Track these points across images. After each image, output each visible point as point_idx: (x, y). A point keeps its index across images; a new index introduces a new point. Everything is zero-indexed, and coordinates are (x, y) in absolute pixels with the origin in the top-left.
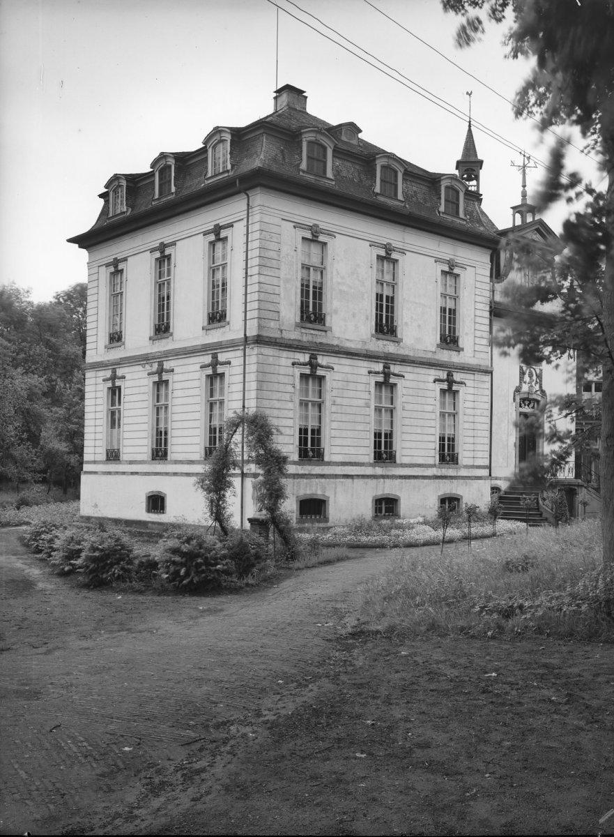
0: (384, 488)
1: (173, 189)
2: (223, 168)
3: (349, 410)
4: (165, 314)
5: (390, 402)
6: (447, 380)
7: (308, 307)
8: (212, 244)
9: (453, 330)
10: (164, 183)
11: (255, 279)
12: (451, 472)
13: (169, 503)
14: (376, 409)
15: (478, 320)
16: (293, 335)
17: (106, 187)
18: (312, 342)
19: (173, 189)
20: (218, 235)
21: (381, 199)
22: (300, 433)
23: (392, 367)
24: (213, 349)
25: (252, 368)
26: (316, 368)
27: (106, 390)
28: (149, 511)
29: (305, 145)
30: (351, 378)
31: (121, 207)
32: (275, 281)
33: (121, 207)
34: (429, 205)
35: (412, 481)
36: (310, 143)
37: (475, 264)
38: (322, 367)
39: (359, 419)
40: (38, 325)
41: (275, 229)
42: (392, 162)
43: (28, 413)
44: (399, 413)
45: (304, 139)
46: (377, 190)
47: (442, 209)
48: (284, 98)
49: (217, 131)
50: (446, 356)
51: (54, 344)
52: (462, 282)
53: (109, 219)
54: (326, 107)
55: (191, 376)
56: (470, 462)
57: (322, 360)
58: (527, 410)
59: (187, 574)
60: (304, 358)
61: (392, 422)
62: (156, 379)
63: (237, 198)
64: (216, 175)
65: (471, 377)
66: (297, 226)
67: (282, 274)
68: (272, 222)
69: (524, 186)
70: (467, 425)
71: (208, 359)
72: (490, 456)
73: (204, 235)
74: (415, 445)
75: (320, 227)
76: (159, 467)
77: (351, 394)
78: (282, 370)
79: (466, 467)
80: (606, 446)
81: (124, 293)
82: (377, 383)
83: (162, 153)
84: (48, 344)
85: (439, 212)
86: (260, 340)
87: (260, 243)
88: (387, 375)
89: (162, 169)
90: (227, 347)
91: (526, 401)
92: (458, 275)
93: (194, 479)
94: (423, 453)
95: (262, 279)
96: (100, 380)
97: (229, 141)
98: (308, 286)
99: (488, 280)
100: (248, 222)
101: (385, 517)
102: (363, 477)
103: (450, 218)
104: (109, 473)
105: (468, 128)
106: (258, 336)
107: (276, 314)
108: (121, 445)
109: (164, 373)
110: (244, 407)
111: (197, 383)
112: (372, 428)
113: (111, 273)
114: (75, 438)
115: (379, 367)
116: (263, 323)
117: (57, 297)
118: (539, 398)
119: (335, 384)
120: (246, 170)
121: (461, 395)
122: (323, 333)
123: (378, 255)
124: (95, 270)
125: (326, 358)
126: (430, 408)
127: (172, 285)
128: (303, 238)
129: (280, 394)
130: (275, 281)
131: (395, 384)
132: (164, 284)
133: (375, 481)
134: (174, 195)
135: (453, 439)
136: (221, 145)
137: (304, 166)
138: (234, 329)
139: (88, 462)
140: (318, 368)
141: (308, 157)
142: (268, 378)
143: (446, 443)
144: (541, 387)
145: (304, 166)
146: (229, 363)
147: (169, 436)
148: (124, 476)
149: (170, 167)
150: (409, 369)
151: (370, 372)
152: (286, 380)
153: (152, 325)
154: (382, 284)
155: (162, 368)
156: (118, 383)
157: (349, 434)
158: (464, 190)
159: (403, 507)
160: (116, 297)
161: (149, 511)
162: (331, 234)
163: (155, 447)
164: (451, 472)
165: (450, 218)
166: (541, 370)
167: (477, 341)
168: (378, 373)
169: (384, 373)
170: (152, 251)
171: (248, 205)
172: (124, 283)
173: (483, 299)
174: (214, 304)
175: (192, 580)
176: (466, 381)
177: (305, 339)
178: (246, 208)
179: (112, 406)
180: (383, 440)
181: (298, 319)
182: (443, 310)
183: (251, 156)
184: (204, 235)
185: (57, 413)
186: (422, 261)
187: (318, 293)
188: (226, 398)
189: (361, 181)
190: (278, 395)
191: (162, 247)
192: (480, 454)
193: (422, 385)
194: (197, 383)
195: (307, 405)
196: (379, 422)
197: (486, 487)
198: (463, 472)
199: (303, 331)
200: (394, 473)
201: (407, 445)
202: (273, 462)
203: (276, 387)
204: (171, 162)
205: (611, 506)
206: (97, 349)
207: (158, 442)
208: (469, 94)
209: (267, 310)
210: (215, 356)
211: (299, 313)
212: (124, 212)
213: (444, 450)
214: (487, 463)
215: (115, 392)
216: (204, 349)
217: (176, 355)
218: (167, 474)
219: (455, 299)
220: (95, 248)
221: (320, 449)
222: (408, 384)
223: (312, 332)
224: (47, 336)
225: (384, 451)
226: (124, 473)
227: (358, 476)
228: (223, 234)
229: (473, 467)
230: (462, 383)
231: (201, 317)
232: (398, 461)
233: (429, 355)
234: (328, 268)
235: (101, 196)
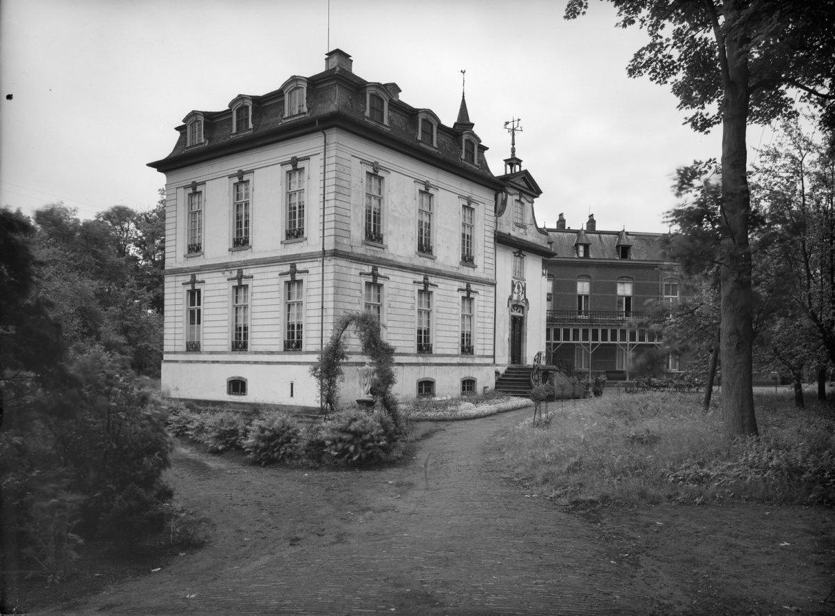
1: (251, 126)
3: (400, 312)
7: (370, 228)
10: (242, 121)
11: (332, 203)
13: (249, 387)
15: (487, 244)
16: (360, 250)
17: (184, 121)
18: (373, 257)
19: (251, 126)
20: (295, 167)
21: (422, 145)
24: (292, 260)
26: (377, 278)
27: (185, 292)
28: (229, 393)
29: (368, 96)
30: (401, 286)
32: (347, 206)
34: (453, 153)
35: (443, 367)
36: (372, 95)
37: (484, 200)
38: (381, 277)
39: (407, 318)
40: (85, 238)
43: (85, 311)
44: (434, 315)
46: (419, 138)
47: (463, 157)
49: (294, 79)
50: (466, 271)
51: (101, 254)
54: (366, 69)
55: (270, 282)
57: (381, 271)
58: (516, 313)
59: (356, 451)
60: (368, 269)
62: (236, 283)
63: (313, 136)
65: (482, 288)
66: (363, 162)
68: (344, 157)
70: (479, 325)
71: (287, 268)
72: (494, 347)
74: (445, 341)
77: (402, 299)
78: (353, 279)
80: (729, 341)
84: (94, 253)
85: (461, 159)
88: (426, 284)
89: (239, 108)
90: (306, 259)
92: (473, 209)
93: (308, 368)
94: (450, 346)
95: (338, 203)
96: (180, 284)
97: (305, 89)
98: (370, 211)
99: (493, 214)
100: (325, 155)
101: (424, 396)
102: (410, 364)
104: (190, 362)
105: (462, 98)
106: (335, 250)
107: (347, 233)
109: (297, 274)
110: (322, 307)
111: (276, 288)
112: (416, 326)
113: (189, 194)
115: (421, 278)
117: (99, 216)
118: (524, 305)
119: (390, 291)
120: (326, 112)
122: (382, 250)
125: (384, 270)
126: (455, 311)
127: (250, 206)
129: (351, 298)
130: (347, 206)
132: (241, 205)
133: (418, 367)
134: (252, 131)
135: (470, 335)
136: (297, 91)
137: (367, 113)
138: (314, 241)
139: (168, 353)
143: (423, 335)
144: (525, 296)
145: (367, 113)
146: (307, 272)
148: (205, 365)
150: (441, 280)
151: (414, 282)
153: (231, 239)
155: (195, 280)
156: (197, 286)
157: (401, 331)
159: (438, 388)
160: (195, 216)
161: (229, 393)
164: (469, 361)
166: (525, 284)
167: (486, 260)
168: (419, 283)
169: (424, 283)
170: (230, 177)
171: (325, 142)
173: (490, 229)
174: (291, 223)
175: (360, 456)
176: (439, 285)
177: (369, 254)
181: (364, 238)
182: (464, 235)
185: (112, 311)
186: (450, 195)
191: (241, 174)
192: (487, 347)
193: (449, 293)
194: (276, 288)
196: (420, 322)
198: (477, 361)
199: (368, 247)
200: (431, 361)
201: (440, 339)
203: (348, 292)
204: (249, 103)
206: (175, 255)
208: (463, 72)
209: (341, 231)
210: (293, 266)
211: (364, 233)
214: (492, 354)
215: (194, 296)
216: (283, 260)
217: (256, 264)
218: (248, 362)
219: (471, 227)
220: (173, 173)
223: (374, 248)
224: (95, 247)
226: (205, 362)
228: (300, 165)
230: (477, 292)
231: (280, 234)
232: (434, 352)
233: (455, 270)
234: (385, 197)
235: (177, 129)
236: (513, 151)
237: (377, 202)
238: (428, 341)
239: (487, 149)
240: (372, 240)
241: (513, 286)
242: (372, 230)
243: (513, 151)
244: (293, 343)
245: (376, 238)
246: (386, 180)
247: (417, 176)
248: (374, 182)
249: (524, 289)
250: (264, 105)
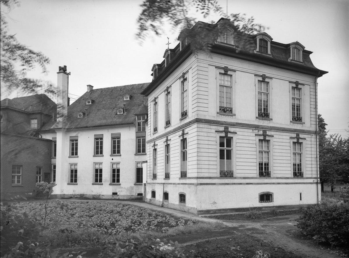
5: (300, 150)
6: (224, 131)
7: (294, 114)
13: (275, 197)
14: (293, 154)
22: (260, 165)
26: (299, 139)
42: (264, 37)
44: (271, 153)
61: (301, 159)
75: (229, 68)
86: (198, 121)
88: (298, 138)
98: (294, 106)
112: (293, 162)
123: (292, 87)
128: (258, 80)
131: (302, 143)
140: (300, 139)
141: (260, 46)
151: (216, 131)
154: (294, 99)
158: (270, 41)
176: (306, 138)
180: (297, 167)
195: (295, 154)
205: (71, 200)
218: (274, 183)
221: (268, 172)
222: (275, 140)
225: (264, 171)
237: (266, 97)
238: (301, 170)
239: (311, 53)
240: (296, 121)
242: (296, 115)
244: (298, 173)
245: (298, 119)
246: (270, 83)
247: (217, 65)
248: (296, 92)
250: (177, 51)
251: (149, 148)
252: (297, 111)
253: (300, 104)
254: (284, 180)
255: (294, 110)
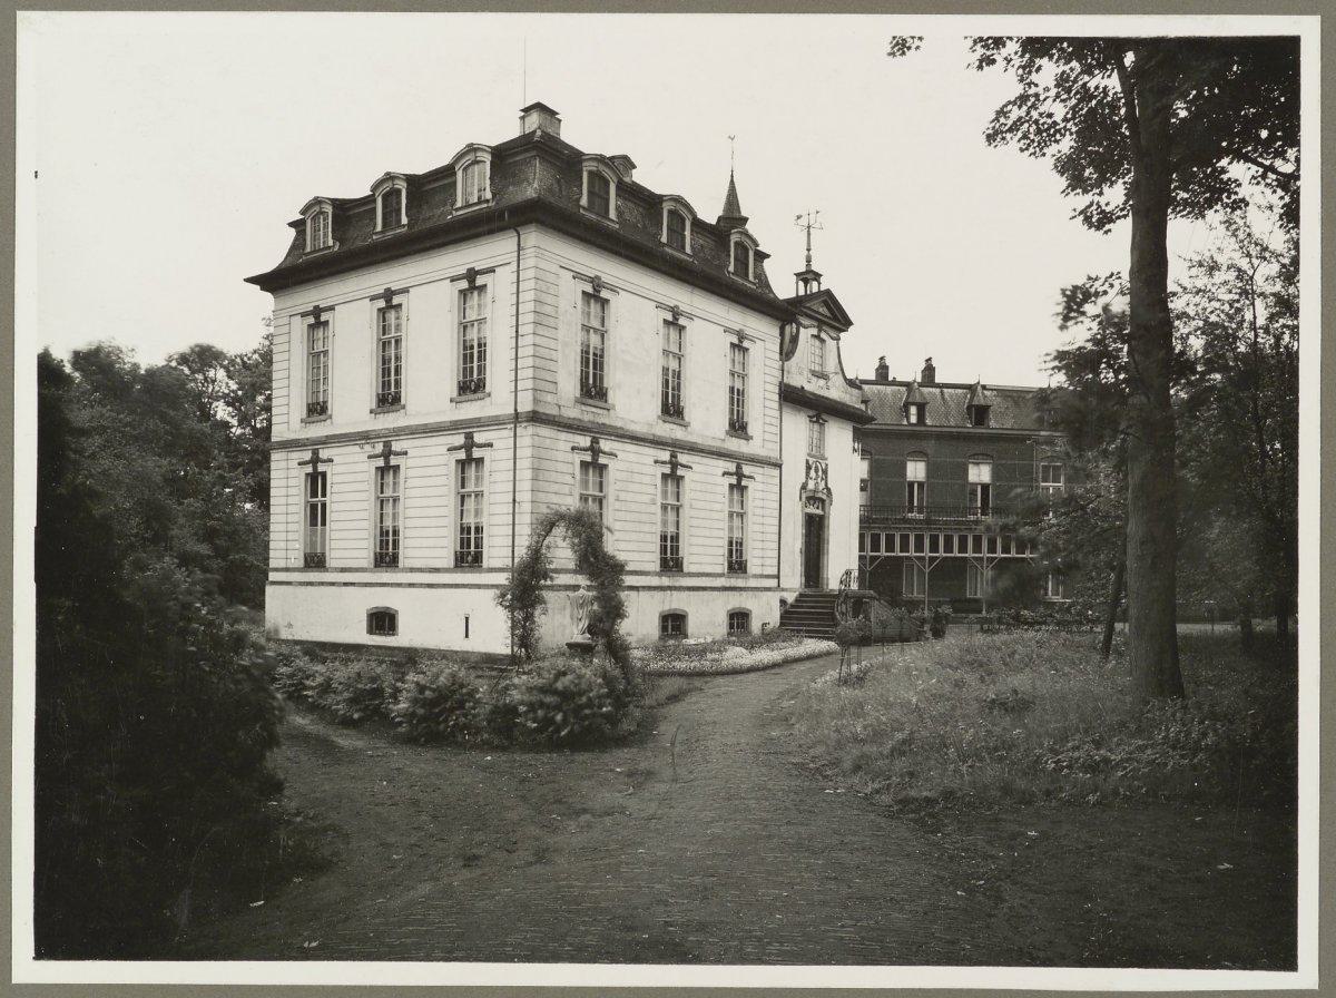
0: (671, 601)
1: (404, 220)
2: (324, 242)
3: (633, 507)
4: (393, 382)
8: (463, 293)
9: (740, 415)
11: (529, 340)
12: (740, 583)
16: (572, 412)
17: (303, 212)
18: (593, 423)
19: (404, 220)
20: (472, 283)
23: (679, 456)
24: (467, 427)
25: (525, 452)
28: (371, 631)
29: (585, 175)
30: (636, 468)
31: (326, 239)
32: (552, 344)
33: (326, 239)
37: (764, 333)
38: (604, 453)
41: (551, 278)
42: (679, 207)
44: (685, 512)
45: (584, 169)
48: (534, 120)
50: (735, 445)
52: (751, 357)
53: (307, 254)
55: (433, 461)
56: (282, 564)
57: (605, 445)
58: (812, 510)
60: (585, 441)
64: (480, 202)
66: (577, 276)
67: (560, 334)
69: (809, 250)
70: (757, 528)
73: (452, 281)
76: (386, 577)
79: (755, 576)
81: (330, 352)
82: (663, 474)
83: (388, 174)
85: (729, 272)
87: (536, 295)
88: (674, 465)
89: (387, 192)
90: (488, 425)
91: (813, 499)
93: (492, 593)
95: (539, 340)
97: (488, 163)
99: (777, 357)
100: (519, 266)
101: (671, 637)
102: (650, 588)
103: (740, 281)
108: (327, 548)
111: (443, 470)
112: (658, 529)
114: (254, 538)
116: (538, 395)
118: (824, 497)
121: (750, 493)
122: (605, 412)
124: (286, 320)
125: (608, 442)
127: (403, 343)
132: (390, 342)
135: (741, 544)
137: (584, 201)
138: (500, 396)
139: (276, 570)
142: (546, 465)
143: (669, 543)
145: (584, 201)
147: (401, 537)
149: (399, 191)
151: (656, 462)
152: (565, 468)
155: (318, 457)
157: (634, 536)
160: (317, 360)
162: (613, 289)
163: (378, 550)
164: (740, 583)
165: (740, 281)
167: (767, 428)
171: (519, 245)
172: (330, 339)
177: (586, 418)
178: (516, 248)
179: (311, 497)
183: (519, 183)
184: (452, 281)
187: (599, 362)
188: (401, 494)
189: (644, 227)
190: (555, 488)
191: (388, 295)
194: (443, 470)
196: (665, 523)
197: (773, 601)
198: (753, 583)
199: (583, 408)
202: (601, 568)
204: (402, 185)
207: (383, 544)
209: (543, 381)
210: (469, 436)
212: (330, 247)
213: (666, 553)
215: (316, 482)
216: (454, 426)
217: (411, 434)
218: (399, 585)
219: (743, 377)
222: (696, 477)
223: (594, 410)
227: (644, 587)
229: (287, 570)
232: (685, 570)
233: (718, 444)
235: (291, 225)
236: (809, 261)
239: (768, 256)
241: (809, 468)
242: (591, 381)
243: (809, 261)
244: (469, 556)
245: (597, 393)
249: (825, 472)
251: (282, 474)
252: (595, 368)
253: (602, 350)
254: (427, 575)
255: (587, 366)
